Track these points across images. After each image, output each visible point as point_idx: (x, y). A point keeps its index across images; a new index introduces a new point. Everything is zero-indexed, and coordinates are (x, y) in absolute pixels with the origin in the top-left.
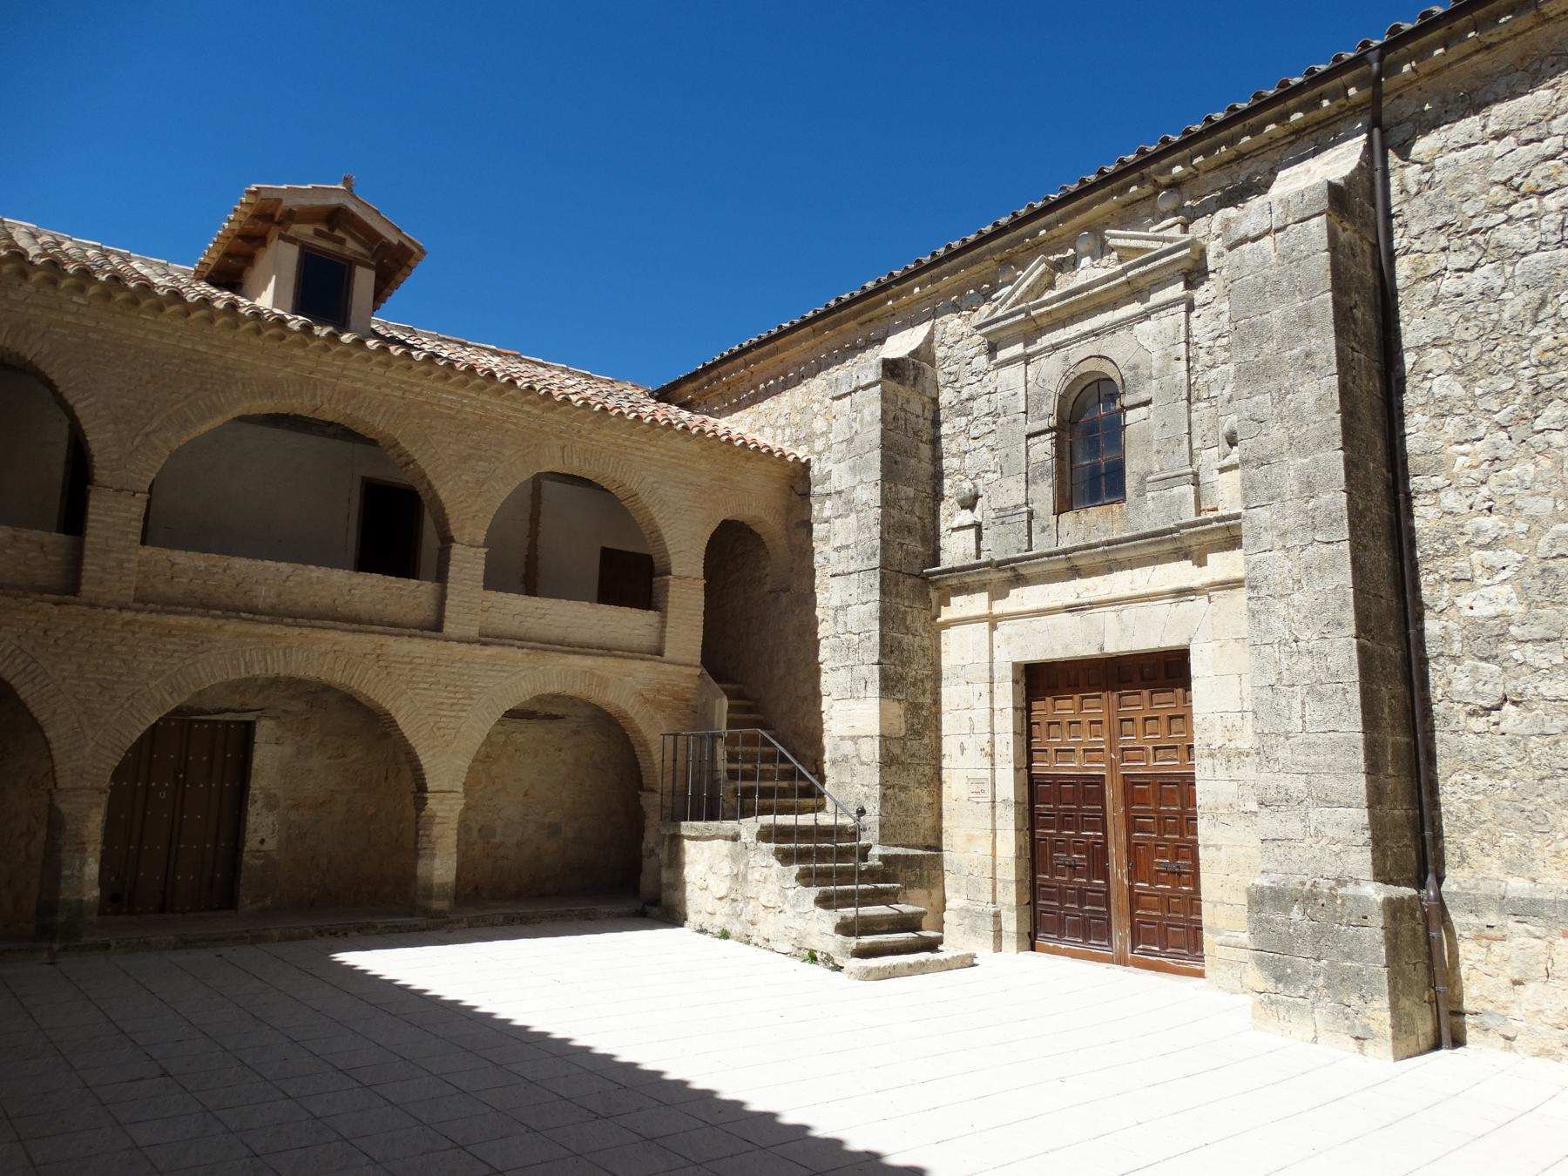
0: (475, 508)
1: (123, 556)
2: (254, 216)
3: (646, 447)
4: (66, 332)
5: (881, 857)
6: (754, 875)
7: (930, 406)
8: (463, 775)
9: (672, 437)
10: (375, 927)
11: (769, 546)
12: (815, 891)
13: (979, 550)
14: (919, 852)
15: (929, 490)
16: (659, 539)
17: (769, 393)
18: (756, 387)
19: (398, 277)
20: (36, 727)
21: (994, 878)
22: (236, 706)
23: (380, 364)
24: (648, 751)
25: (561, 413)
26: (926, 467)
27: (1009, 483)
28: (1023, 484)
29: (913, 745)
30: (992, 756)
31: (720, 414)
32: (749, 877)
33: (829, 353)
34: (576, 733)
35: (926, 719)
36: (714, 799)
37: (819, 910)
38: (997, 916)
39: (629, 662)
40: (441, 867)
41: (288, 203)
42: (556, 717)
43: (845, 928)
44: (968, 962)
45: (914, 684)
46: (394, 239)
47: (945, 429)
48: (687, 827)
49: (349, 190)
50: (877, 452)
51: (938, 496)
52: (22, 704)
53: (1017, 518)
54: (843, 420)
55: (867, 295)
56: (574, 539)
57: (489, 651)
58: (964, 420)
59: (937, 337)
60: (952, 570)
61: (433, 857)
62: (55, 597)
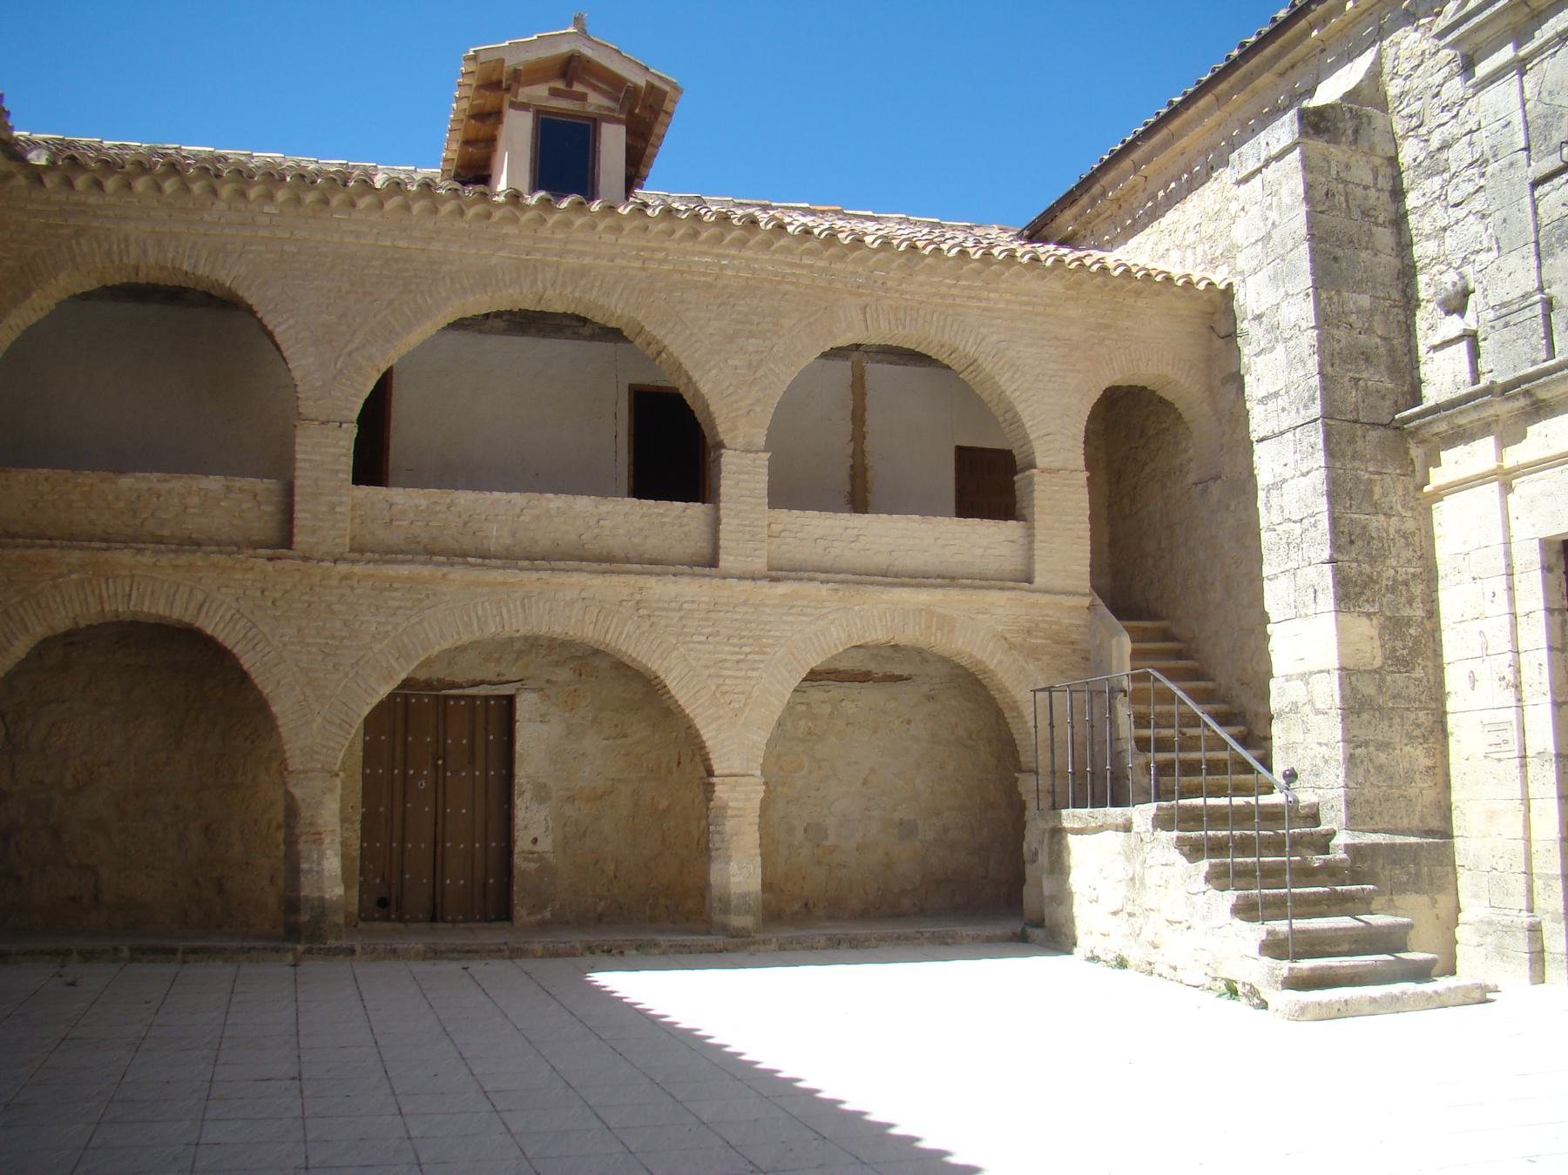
0: (748, 401)
1: (334, 499)
2: (479, 87)
3: (985, 294)
4: (262, 248)
5: (1349, 848)
6: (1152, 878)
7: (1385, 171)
8: (760, 753)
9: (1019, 276)
10: (656, 945)
11: (1187, 416)
12: (1230, 897)
13: (1476, 375)
14: (1413, 840)
15: (1396, 295)
16: (1016, 421)
17: (1172, 201)
18: (1154, 197)
19: (657, 129)
20: (261, 706)
21: (1528, 873)
22: (492, 677)
23: (609, 229)
24: (1020, 716)
25: (854, 261)
26: (1387, 261)
27: (1512, 261)
28: (1533, 261)
29: (1397, 680)
30: (1517, 687)
31: (1111, 245)
32: (1148, 882)
33: (1243, 126)
34: (930, 698)
35: (1416, 641)
36: (1119, 777)
37: (1237, 922)
38: (1535, 930)
39: (981, 593)
40: (740, 872)
41: (511, 62)
42: (899, 678)
43: (1274, 948)
44: (1481, 996)
45: (1392, 589)
46: (640, 80)
47: (1412, 201)
48: (1071, 817)
49: (583, 33)
50: (1304, 248)
51: (1410, 303)
52: (244, 677)
53: (1527, 313)
54: (1254, 211)
55: (1280, 28)
56: (917, 440)
57: (782, 588)
58: (1437, 182)
59: (1387, 67)
60: (1436, 409)
61: (728, 859)
62: (269, 552)
